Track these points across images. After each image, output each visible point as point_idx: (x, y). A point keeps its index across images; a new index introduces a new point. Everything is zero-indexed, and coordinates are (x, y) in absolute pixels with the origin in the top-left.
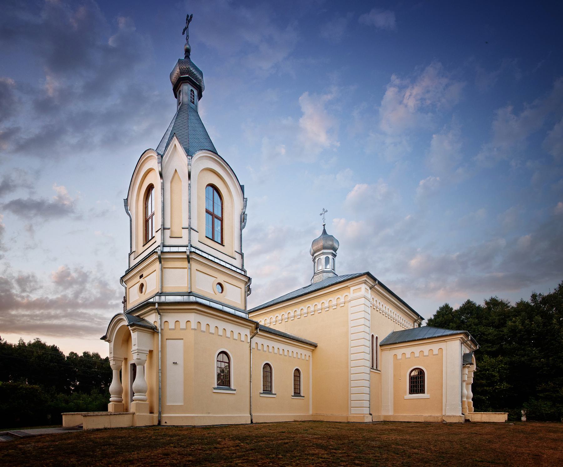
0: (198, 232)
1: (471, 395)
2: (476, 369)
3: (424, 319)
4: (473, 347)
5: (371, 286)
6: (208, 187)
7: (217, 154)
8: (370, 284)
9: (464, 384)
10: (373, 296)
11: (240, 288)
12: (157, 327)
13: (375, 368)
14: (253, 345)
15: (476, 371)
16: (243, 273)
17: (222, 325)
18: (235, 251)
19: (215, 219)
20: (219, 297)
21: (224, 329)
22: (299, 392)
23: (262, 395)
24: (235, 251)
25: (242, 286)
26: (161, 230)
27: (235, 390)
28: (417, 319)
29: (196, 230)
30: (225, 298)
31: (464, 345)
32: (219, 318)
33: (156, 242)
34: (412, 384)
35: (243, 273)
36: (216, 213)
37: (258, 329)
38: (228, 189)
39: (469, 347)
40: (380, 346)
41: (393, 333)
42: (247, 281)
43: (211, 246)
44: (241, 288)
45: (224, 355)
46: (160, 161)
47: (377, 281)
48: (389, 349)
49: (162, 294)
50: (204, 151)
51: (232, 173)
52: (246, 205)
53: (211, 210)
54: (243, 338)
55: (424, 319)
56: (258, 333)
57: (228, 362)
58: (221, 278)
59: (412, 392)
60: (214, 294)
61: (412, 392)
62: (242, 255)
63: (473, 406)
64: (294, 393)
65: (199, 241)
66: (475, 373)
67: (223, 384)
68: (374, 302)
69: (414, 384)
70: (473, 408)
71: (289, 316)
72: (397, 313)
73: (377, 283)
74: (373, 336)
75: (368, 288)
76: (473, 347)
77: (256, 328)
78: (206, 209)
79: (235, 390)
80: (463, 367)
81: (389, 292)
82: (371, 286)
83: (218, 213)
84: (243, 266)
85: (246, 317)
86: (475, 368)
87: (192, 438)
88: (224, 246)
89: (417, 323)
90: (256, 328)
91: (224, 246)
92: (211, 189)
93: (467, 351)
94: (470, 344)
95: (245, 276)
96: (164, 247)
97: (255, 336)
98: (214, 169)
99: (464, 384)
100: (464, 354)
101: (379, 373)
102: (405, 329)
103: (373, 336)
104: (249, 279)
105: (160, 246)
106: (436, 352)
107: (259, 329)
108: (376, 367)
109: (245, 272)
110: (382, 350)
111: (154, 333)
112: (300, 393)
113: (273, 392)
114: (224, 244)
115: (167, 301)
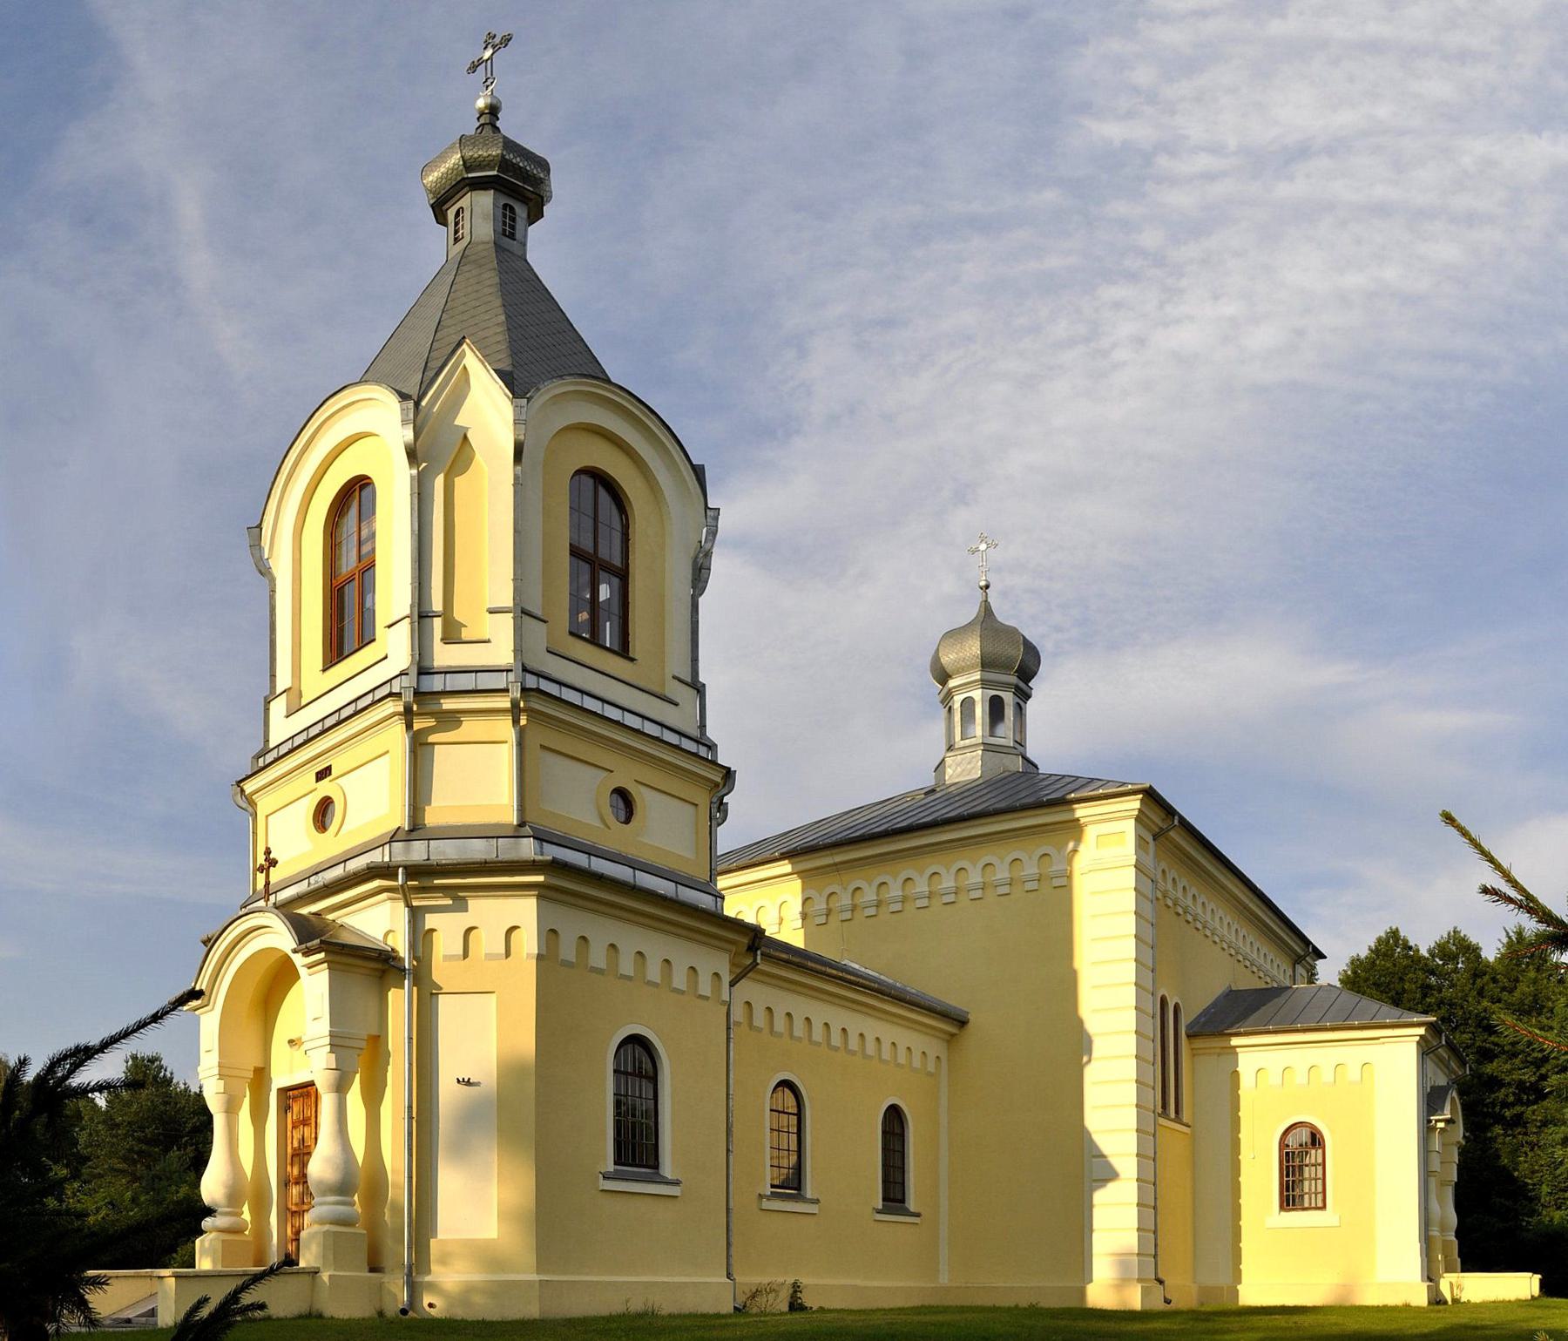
0: (545, 622)
1: (1453, 1219)
2: (1464, 1137)
3: (1325, 957)
4: (1456, 1069)
5: (1157, 830)
6: (577, 477)
7: (608, 381)
8: (1154, 822)
9: (1433, 1182)
10: (1163, 865)
11: (693, 804)
12: (397, 951)
13: (1173, 1115)
14: (738, 1014)
15: (1464, 1143)
16: (703, 751)
17: (631, 939)
18: (674, 677)
19: (601, 572)
20: (617, 837)
21: (639, 953)
22: (900, 1197)
23: (766, 1204)
24: (674, 677)
25: (703, 798)
26: (412, 623)
27: (676, 1183)
28: (1302, 953)
29: (539, 613)
30: (639, 839)
31: (1432, 1060)
32: (617, 912)
33: (386, 657)
34: (1288, 1176)
35: (703, 751)
36: (603, 553)
37: (759, 952)
38: (648, 481)
39: (1444, 1064)
40: (1188, 1036)
41: (1227, 995)
42: (719, 780)
43: (588, 662)
44: (696, 805)
45: (638, 1049)
46: (411, 416)
47: (1176, 817)
48: (1218, 1051)
49: (415, 835)
50: (569, 379)
51: (664, 434)
52: (717, 530)
53: (587, 545)
54: (705, 987)
55: (1325, 957)
56: (759, 967)
57: (708, 511)
58: (626, 774)
59: (1288, 1205)
60: (602, 826)
61: (1288, 1205)
62: (700, 690)
63: (1459, 1256)
64: (884, 1200)
65: (548, 651)
66: (1463, 1152)
67: (634, 1159)
68: (1166, 883)
69: (1294, 1175)
70: (1459, 1260)
71: (881, 897)
72: (1241, 928)
73: (1176, 822)
74: (1163, 1001)
75: (1150, 838)
76: (1456, 1069)
77: (752, 949)
78: (571, 545)
79: (676, 1183)
80: (1428, 1128)
81: (1215, 855)
82: (1157, 830)
83: (610, 551)
84: (703, 726)
85: (714, 909)
86: (1462, 1135)
87: (1540, 1127)
88: (632, 660)
89: (1304, 967)
90: (752, 949)
91: (632, 660)
92: (588, 482)
93: (1442, 1081)
94: (1447, 1057)
95: (714, 763)
96: (423, 677)
97: (744, 976)
98: (598, 424)
99: (1433, 1182)
100: (1431, 1087)
101: (917, 1224)
102: (1264, 986)
103: (1163, 1001)
104: (729, 775)
105: (407, 674)
106: (1353, 1072)
107: (762, 954)
108: (1177, 1112)
109: (711, 747)
110: (1195, 1052)
111: (384, 971)
112: (903, 1201)
113: (809, 1195)
114: (631, 655)
115: (435, 858)
